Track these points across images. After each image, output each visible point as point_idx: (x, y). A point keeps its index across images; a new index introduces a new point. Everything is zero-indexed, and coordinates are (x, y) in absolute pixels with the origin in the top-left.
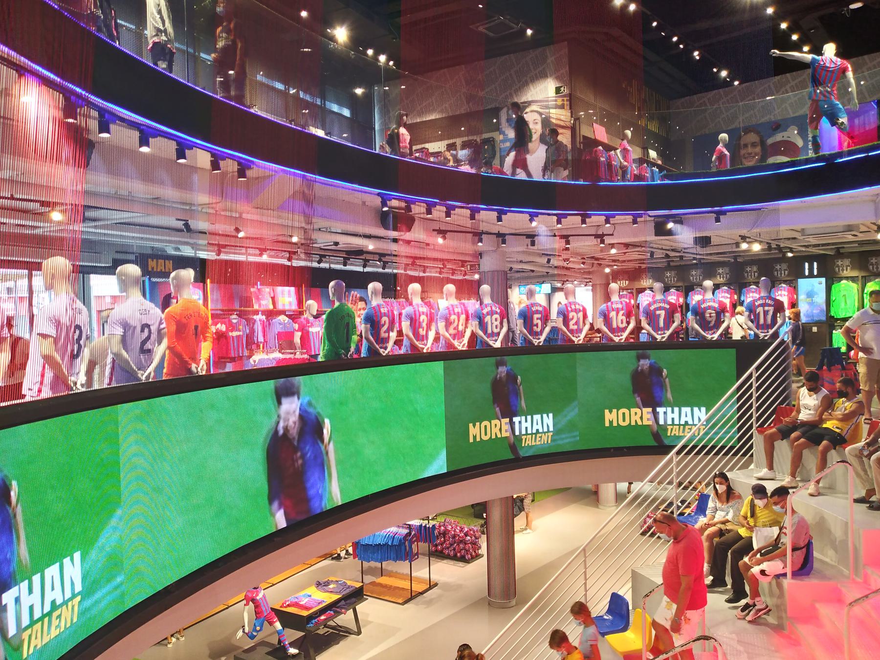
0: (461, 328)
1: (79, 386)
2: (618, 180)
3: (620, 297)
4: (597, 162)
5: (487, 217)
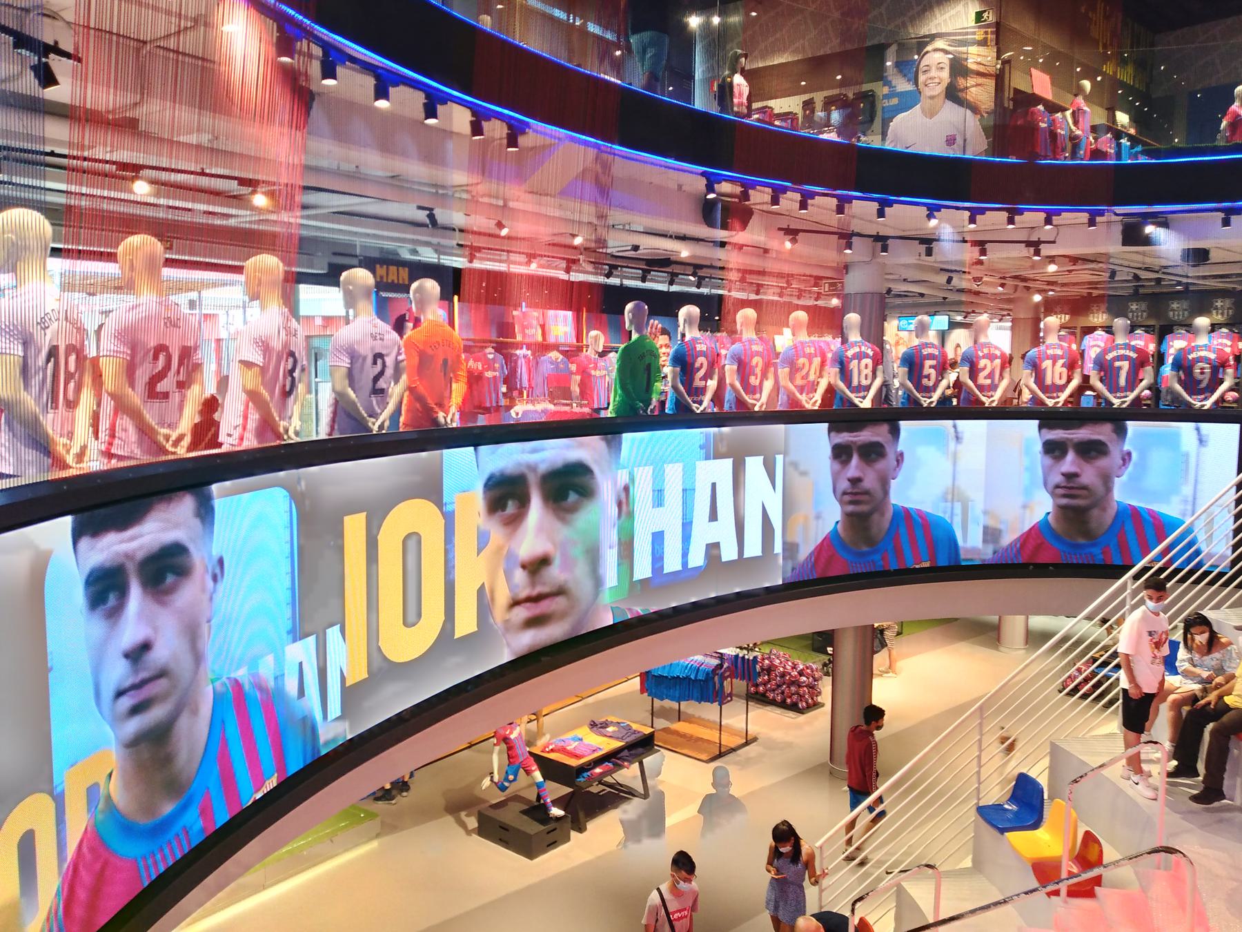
0: (812, 377)
1: (291, 433)
2: (1066, 158)
3: (1060, 338)
4: (1034, 129)
5: (863, 210)
